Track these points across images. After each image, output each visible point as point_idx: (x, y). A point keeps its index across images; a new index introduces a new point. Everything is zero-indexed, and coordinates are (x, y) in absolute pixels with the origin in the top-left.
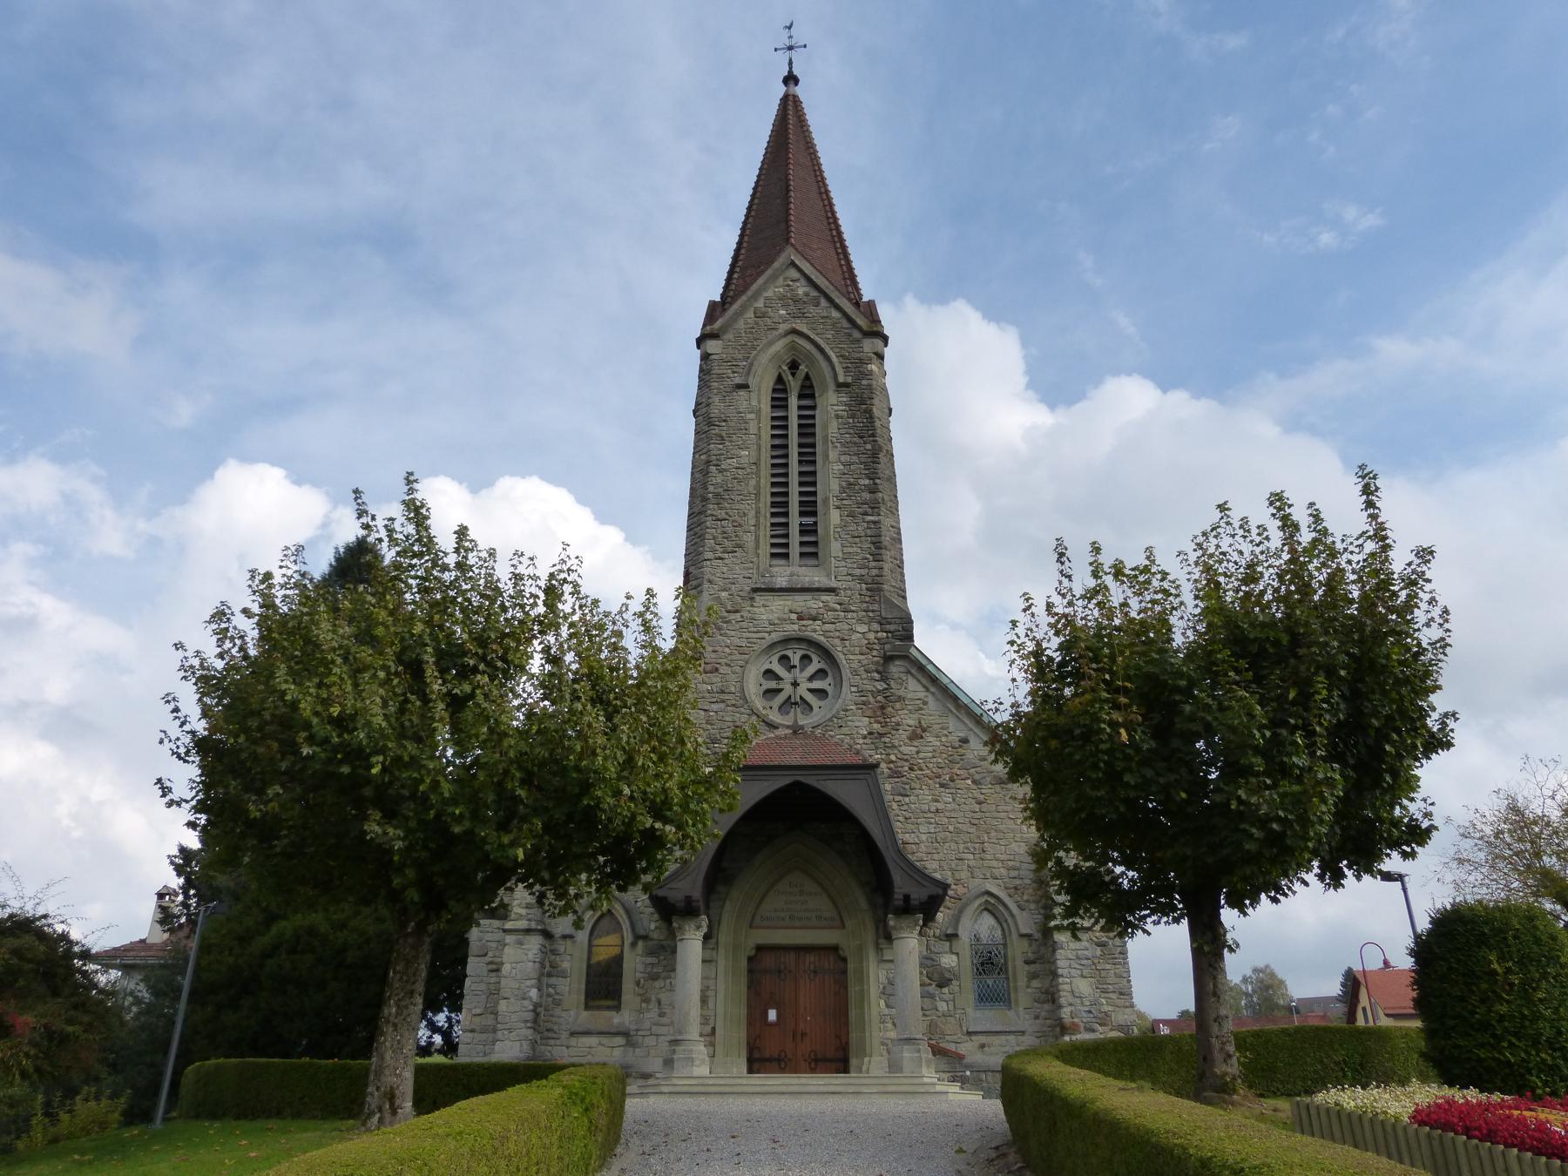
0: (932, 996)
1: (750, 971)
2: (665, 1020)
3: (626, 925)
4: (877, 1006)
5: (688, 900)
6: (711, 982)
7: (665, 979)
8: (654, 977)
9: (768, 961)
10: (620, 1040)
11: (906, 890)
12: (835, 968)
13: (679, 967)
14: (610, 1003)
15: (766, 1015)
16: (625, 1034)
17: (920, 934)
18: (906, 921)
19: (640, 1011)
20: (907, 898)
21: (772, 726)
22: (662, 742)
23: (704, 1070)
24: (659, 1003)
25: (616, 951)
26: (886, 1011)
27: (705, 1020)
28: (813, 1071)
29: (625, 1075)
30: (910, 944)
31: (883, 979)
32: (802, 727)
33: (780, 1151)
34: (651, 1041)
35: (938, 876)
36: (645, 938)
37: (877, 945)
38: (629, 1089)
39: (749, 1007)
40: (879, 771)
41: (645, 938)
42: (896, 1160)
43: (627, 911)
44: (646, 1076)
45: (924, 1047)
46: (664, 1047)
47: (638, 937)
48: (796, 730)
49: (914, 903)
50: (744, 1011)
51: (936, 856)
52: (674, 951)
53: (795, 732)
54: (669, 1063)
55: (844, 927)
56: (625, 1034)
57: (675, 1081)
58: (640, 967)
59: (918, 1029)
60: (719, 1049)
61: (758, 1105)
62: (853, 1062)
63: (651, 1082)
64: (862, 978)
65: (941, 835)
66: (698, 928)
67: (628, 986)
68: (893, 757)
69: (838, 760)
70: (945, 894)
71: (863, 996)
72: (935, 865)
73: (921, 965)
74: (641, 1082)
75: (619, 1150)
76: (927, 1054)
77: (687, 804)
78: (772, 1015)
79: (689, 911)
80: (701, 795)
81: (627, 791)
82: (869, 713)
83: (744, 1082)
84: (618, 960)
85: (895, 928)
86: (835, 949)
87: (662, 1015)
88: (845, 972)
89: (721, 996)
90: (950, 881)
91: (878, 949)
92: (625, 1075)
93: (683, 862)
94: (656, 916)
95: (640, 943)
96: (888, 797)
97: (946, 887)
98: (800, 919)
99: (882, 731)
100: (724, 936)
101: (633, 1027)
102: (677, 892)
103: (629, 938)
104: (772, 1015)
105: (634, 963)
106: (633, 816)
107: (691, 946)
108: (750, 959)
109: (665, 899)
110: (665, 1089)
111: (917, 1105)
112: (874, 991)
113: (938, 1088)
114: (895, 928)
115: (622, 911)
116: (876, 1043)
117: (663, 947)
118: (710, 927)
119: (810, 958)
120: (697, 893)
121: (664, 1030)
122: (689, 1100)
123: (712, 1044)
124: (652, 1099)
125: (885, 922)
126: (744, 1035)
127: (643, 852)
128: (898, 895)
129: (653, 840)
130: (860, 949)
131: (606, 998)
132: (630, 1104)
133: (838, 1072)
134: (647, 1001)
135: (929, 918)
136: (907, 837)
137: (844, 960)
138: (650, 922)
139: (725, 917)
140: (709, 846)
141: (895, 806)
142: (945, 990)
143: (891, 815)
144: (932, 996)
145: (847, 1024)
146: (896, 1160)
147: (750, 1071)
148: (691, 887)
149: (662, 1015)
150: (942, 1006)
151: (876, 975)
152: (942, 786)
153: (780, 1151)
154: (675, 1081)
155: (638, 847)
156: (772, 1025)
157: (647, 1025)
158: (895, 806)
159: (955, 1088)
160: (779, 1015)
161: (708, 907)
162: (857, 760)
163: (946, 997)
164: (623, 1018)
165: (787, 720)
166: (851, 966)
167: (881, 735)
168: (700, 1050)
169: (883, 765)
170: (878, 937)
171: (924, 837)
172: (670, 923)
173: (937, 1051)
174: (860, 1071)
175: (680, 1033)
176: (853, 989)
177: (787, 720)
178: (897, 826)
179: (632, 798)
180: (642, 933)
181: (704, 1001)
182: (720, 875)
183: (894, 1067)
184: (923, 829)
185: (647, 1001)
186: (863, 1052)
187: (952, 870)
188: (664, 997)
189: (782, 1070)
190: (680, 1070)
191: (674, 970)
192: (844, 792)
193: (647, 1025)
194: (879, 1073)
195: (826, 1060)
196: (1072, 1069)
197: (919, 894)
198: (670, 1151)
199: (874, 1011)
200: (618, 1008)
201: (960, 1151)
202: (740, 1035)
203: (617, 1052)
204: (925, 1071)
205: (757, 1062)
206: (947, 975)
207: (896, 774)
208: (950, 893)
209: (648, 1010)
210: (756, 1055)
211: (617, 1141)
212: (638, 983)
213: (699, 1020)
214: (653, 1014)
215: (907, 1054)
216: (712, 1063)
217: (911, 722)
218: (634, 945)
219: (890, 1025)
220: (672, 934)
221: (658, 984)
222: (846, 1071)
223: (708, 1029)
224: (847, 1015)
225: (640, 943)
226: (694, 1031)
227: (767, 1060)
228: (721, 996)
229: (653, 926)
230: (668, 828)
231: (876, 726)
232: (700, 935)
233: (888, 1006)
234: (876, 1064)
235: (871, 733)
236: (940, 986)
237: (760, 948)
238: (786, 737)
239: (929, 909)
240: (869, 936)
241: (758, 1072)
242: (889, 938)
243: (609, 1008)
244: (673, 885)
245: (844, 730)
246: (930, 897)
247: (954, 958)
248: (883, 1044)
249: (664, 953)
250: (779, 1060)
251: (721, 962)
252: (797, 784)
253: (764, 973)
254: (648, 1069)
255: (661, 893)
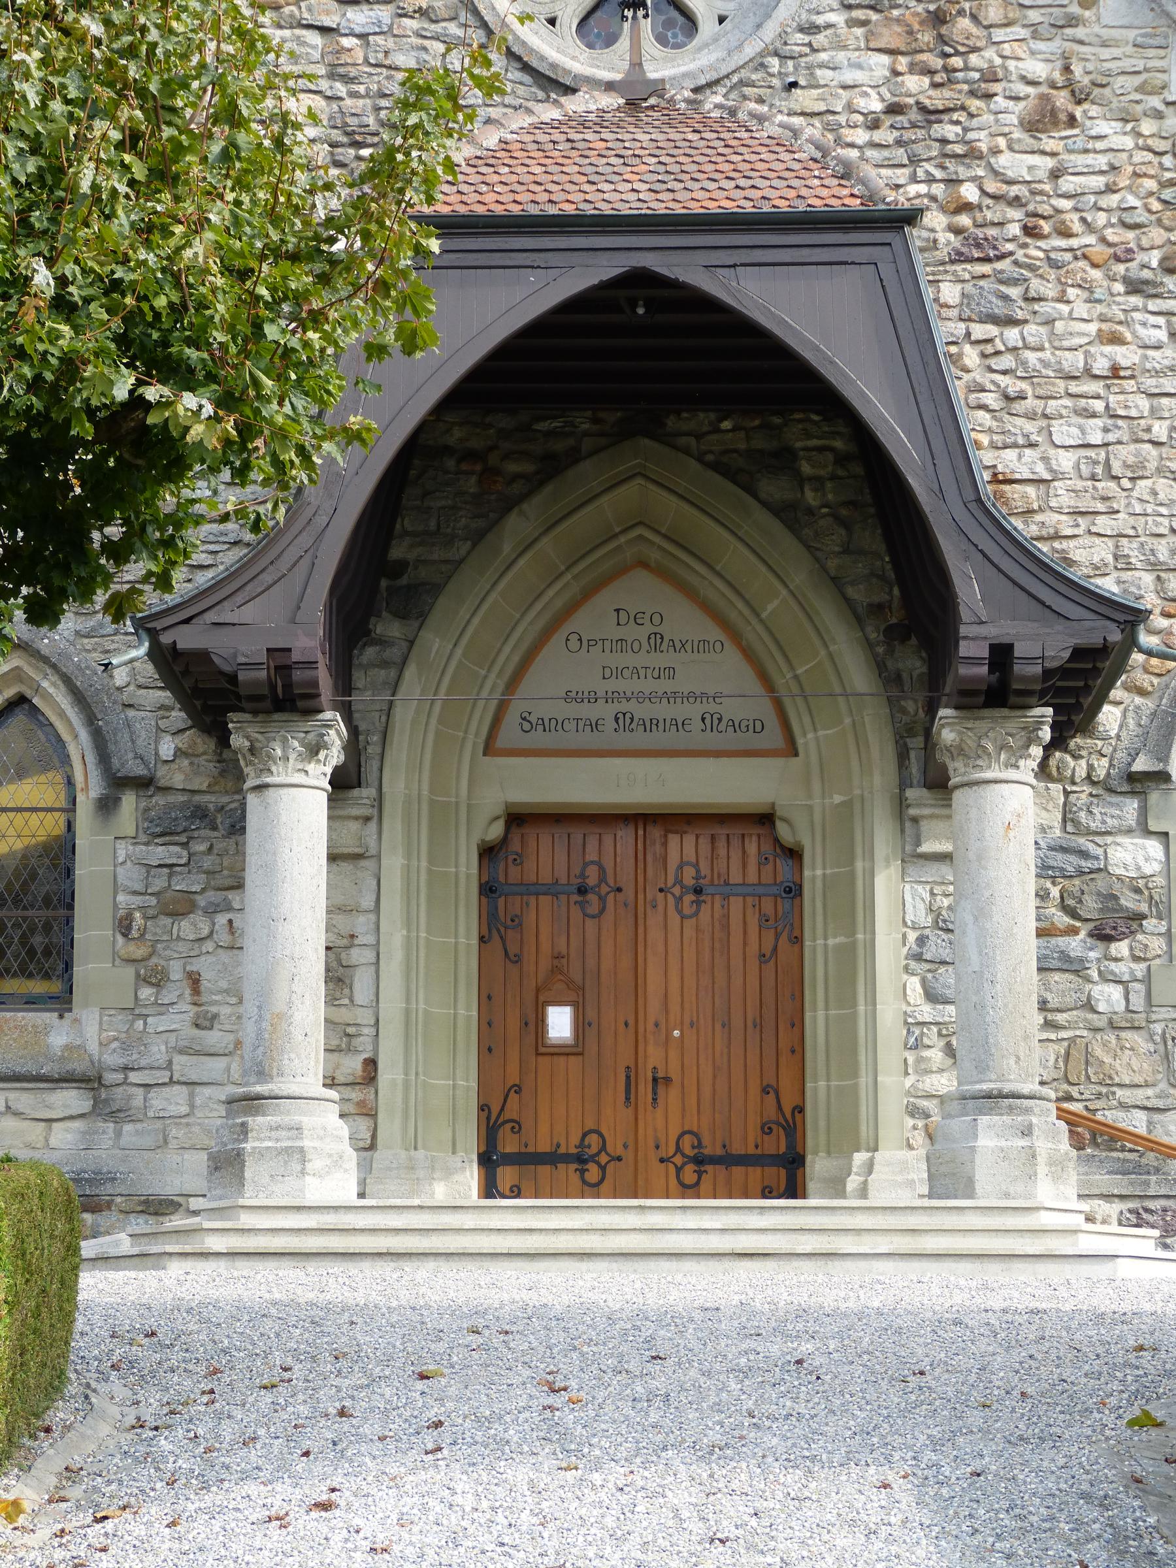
0: (1075, 967)
1: (488, 890)
2: (214, 1038)
3: (79, 746)
4: (895, 993)
5: (281, 661)
6: (362, 924)
7: (212, 911)
8: (178, 907)
9: (547, 856)
10: (71, 1100)
11: (1000, 630)
12: (769, 882)
13: (252, 877)
14: (37, 987)
15: (541, 1022)
16: (89, 1080)
17: (1043, 771)
18: (998, 727)
19: (135, 1011)
20: (1001, 655)
21: (553, 84)
22: (160, 110)
23: (339, 1185)
24: (194, 981)
25: (53, 825)
26: (926, 1012)
27: (341, 1036)
28: (689, 1190)
29: (83, 1200)
30: (1011, 805)
31: (918, 913)
32: (658, 87)
33: (568, 1417)
34: (173, 1101)
35: (1108, 585)
36: (144, 784)
37: (901, 804)
38: (88, 1248)
39: (486, 999)
40: (916, 236)
41: (144, 784)
42: (935, 1444)
43: (79, 697)
44: (158, 1207)
45: (1044, 1117)
46: (213, 1116)
47: (118, 783)
48: (639, 97)
49: (1025, 671)
50: (468, 1010)
51: (1103, 524)
52: (238, 828)
53: (633, 104)
54: (228, 1164)
55: (792, 749)
56: (89, 1080)
57: (247, 1220)
58: (130, 876)
59: (1024, 1057)
60: (389, 1127)
61: (508, 1288)
62: (817, 1166)
63: (177, 1221)
64: (852, 910)
65: (1126, 453)
66: (314, 750)
67: (92, 931)
68: (969, 192)
69: (779, 198)
70: (1131, 643)
71: (854, 963)
72: (1102, 552)
73: (1045, 871)
74: (141, 1224)
75: (59, 1414)
76: (1052, 1139)
77: (257, 326)
78: (560, 1023)
79: (285, 697)
80: (299, 298)
81: (43, 278)
82: (891, 37)
83: (468, 1220)
84: (60, 854)
85: (959, 751)
86: (765, 819)
87: (205, 1022)
88: (794, 891)
89: (392, 968)
90: (1150, 601)
91: (905, 820)
92: (83, 1200)
93: (245, 539)
94: (178, 717)
95: (129, 801)
96: (946, 329)
97: (1131, 618)
98: (650, 725)
99: (936, 99)
100: (400, 778)
101: (112, 1059)
102: (244, 637)
103: (90, 786)
104: (560, 1023)
105: (111, 865)
106: (70, 365)
107: (295, 807)
108: (488, 853)
109: (203, 656)
110: (216, 1243)
111: (1017, 1289)
112: (888, 949)
113: (1087, 1244)
114: (959, 751)
115: (63, 700)
116: (891, 1106)
117: (201, 814)
118: (353, 747)
119: (682, 848)
120: (309, 641)
121: (214, 1067)
122: (289, 1272)
123: (370, 1113)
124: (176, 1268)
125: (930, 743)
126: (468, 1083)
127: (107, 493)
128: (972, 647)
129: (144, 451)
130: (846, 824)
131: (25, 972)
132: (92, 1285)
133: (767, 1192)
134: (157, 979)
135: (1074, 719)
136: (1009, 462)
137: (794, 854)
138: (160, 734)
139: (403, 715)
140: (343, 473)
141: (971, 356)
142: (1121, 948)
143: (958, 389)
144: (1075, 967)
145: (798, 1050)
146: (935, 1444)
147: (489, 1189)
148: (288, 618)
149: (205, 1022)
150: (1109, 997)
151: (897, 901)
152: (1135, 287)
153: (568, 1417)
154: (247, 1220)
155: (91, 474)
156: (561, 1051)
157: (158, 1052)
158: (971, 356)
159: (1145, 1241)
160: (580, 1024)
161: (344, 684)
162: (846, 199)
163: (1121, 969)
164: (81, 1031)
165: (609, 65)
166: (814, 873)
167: (931, 115)
168: (326, 1127)
169: (935, 220)
170: (904, 784)
171: (1065, 461)
172: (223, 740)
173: (1090, 1135)
174: (837, 1187)
175: (262, 1074)
176: (820, 943)
177: (609, 65)
178: (977, 425)
179: (62, 305)
180: (137, 769)
181: (338, 977)
182: (382, 581)
183: (949, 1179)
184: (1064, 432)
185: (157, 979)
186: (853, 1135)
187: (1154, 566)
188: (206, 967)
189: (593, 1189)
190: (262, 1184)
191: (239, 886)
192: (809, 312)
193: (158, 1052)
194: (905, 1198)
195: (728, 1160)
196: (121, 1273)
197: (1042, 645)
198: (219, 1416)
199: (888, 1014)
200: (62, 1002)
201: (1145, 1421)
202: (457, 1083)
203: (64, 1137)
204: (1045, 1191)
205: (513, 1159)
206: (1129, 901)
207: (977, 249)
208: (1146, 639)
209: (162, 1008)
210: (509, 1144)
211: (54, 1386)
212: (124, 926)
213: (319, 1036)
214: (177, 1019)
215: (990, 1137)
216: (365, 1169)
217: (1038, 69)
218: (107, 806)
219: (936, 1055)
220: (231, 772)
221: (186, 927)
222: (794, 1189)
223: (353, 1065)
224: (797, 1022)
225: (129, 801)
226: (304, 1063)
227: (552, 1158)
228: (392, 968)
229: (167, 748)
230: (189, 400)
231: (915, 84)
232: (320, 773)
233: (932, 996)
234: (894, 1169)
235: (894, 109)
236: (1103, 936)
237: (518, 818)
238: (601, 121)
239: (1075, 689)
240: (880, 777)
241: (516, 1192)
242: (939, 784)
243: (31, 1002)
244: (225, 614)
245: (804, 99)
246: (1078, 653)
247: (1154, 848)
248: (913, 1111)
249: (210, 829)
250: (581, 1160)
251: (393, 864)
252: (639, 279)
253: (530, 890)
254: (169, 1186)
255: (187, 639)
